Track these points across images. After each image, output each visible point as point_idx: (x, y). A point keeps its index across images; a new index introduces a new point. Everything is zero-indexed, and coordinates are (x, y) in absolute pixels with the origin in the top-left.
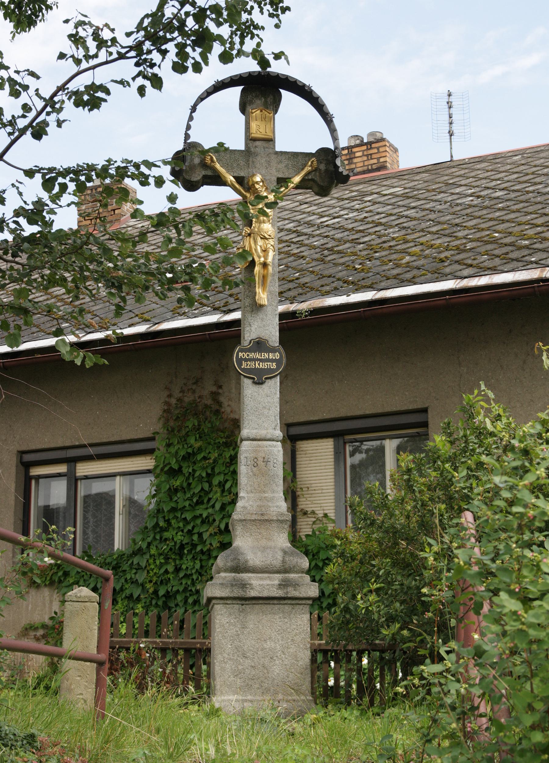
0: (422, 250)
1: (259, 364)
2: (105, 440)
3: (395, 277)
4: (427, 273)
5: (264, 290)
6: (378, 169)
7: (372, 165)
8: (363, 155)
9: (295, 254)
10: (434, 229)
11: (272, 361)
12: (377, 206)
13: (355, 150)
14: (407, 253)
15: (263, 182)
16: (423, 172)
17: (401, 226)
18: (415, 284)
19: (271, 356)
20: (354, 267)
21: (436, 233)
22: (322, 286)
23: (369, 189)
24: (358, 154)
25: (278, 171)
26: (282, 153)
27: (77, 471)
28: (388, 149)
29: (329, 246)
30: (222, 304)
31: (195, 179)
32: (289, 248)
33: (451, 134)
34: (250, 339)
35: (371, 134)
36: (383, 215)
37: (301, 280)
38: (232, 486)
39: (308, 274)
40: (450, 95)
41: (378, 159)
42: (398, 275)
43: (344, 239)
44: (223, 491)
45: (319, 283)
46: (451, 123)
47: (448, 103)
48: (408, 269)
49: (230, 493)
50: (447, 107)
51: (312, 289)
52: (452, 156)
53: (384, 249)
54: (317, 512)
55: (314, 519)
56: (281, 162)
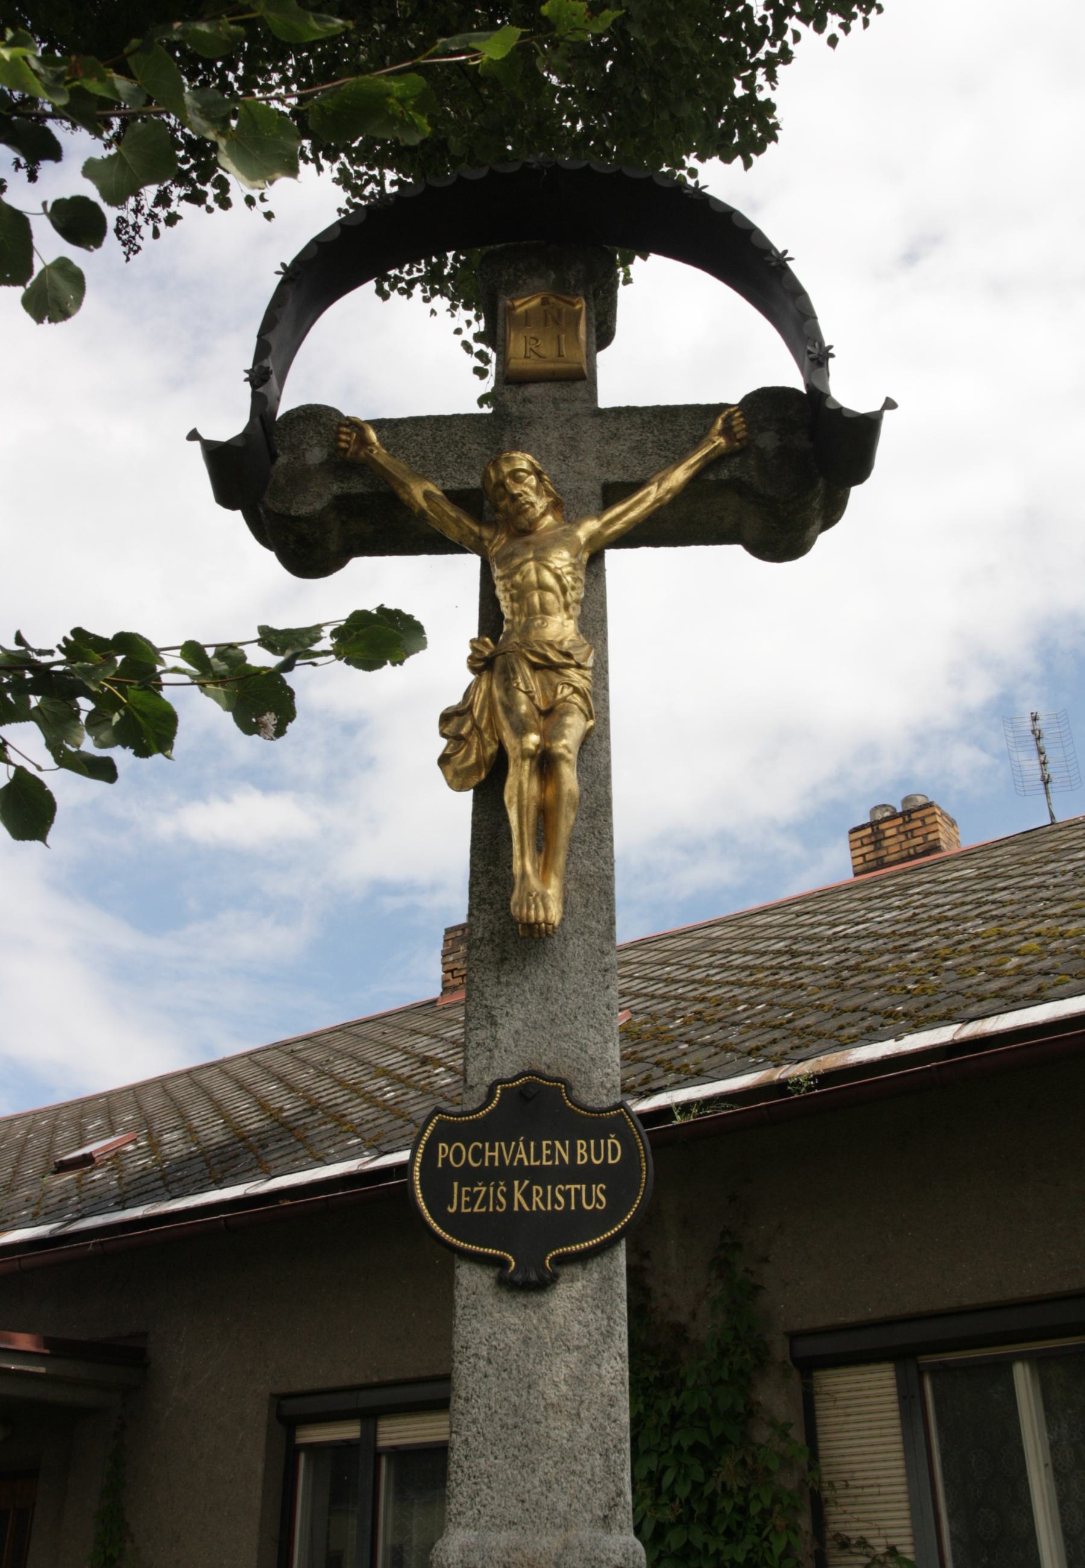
0: (1043, 944)
1: (527, 1195)
2: (426, 1373)
3: (997, 994)
4: (1068, 978)
5: (545, 869)
6: (927, 853)
7: (914, 847)
8: (899, 833)
9: (786, 983)
10: (1058, 910)
11: (588, 1174)
12: (933, 897)
13: (883, 826)
14: (1011, 952)
15: (539, 474)
16: (1006, 845)
17: (987, 915)
18: (1046, 1000)
19: (584, 1152)
20: (905, 988)
21: (1064, 914)
22: (841, 1028)
23: (915, 879)
24: (889, 833)
25: (606, 463)
26: (618, 413)
27: (380, 1436)
28: (939, 819)
29: (852, 962)
30: (639, 1081)
31: (304, 510)
32: (777, 977)
33: (1046, 782)
34: (488, 1079)
35: (907, 800)
36: (948, 907)
37: (796, 1023)
38: (675, 1481)
39: (811, 1011)
40: (1035, 719)
41: (925, 836)
42: (1002, 989)
43: (880, 948)
44: (658, 1493)
45: (835, 1023)
46: (1044, 763)
47: (1033, 732)
48: (1023, 977)
49: (673, 1499)
50: (1033, 737)
51: (820, 1035)
52: (1052, 817)
53: (961, 953)
54: (872, 1542)
55: (867, 1560)
56: (615, 436)
